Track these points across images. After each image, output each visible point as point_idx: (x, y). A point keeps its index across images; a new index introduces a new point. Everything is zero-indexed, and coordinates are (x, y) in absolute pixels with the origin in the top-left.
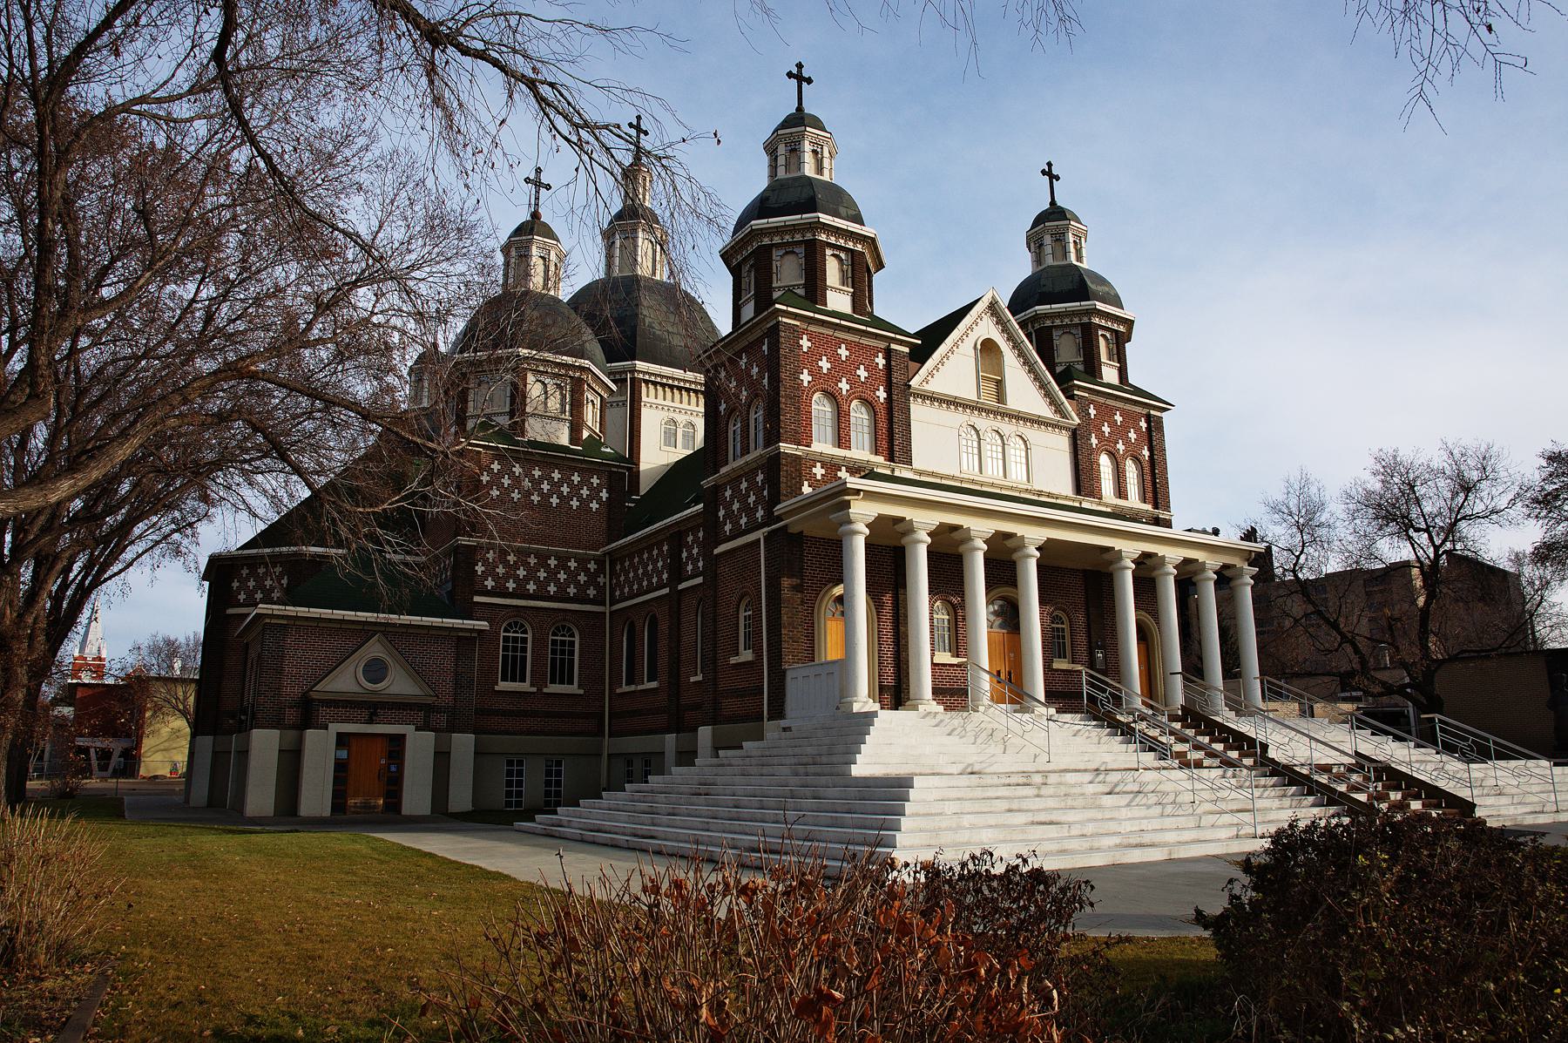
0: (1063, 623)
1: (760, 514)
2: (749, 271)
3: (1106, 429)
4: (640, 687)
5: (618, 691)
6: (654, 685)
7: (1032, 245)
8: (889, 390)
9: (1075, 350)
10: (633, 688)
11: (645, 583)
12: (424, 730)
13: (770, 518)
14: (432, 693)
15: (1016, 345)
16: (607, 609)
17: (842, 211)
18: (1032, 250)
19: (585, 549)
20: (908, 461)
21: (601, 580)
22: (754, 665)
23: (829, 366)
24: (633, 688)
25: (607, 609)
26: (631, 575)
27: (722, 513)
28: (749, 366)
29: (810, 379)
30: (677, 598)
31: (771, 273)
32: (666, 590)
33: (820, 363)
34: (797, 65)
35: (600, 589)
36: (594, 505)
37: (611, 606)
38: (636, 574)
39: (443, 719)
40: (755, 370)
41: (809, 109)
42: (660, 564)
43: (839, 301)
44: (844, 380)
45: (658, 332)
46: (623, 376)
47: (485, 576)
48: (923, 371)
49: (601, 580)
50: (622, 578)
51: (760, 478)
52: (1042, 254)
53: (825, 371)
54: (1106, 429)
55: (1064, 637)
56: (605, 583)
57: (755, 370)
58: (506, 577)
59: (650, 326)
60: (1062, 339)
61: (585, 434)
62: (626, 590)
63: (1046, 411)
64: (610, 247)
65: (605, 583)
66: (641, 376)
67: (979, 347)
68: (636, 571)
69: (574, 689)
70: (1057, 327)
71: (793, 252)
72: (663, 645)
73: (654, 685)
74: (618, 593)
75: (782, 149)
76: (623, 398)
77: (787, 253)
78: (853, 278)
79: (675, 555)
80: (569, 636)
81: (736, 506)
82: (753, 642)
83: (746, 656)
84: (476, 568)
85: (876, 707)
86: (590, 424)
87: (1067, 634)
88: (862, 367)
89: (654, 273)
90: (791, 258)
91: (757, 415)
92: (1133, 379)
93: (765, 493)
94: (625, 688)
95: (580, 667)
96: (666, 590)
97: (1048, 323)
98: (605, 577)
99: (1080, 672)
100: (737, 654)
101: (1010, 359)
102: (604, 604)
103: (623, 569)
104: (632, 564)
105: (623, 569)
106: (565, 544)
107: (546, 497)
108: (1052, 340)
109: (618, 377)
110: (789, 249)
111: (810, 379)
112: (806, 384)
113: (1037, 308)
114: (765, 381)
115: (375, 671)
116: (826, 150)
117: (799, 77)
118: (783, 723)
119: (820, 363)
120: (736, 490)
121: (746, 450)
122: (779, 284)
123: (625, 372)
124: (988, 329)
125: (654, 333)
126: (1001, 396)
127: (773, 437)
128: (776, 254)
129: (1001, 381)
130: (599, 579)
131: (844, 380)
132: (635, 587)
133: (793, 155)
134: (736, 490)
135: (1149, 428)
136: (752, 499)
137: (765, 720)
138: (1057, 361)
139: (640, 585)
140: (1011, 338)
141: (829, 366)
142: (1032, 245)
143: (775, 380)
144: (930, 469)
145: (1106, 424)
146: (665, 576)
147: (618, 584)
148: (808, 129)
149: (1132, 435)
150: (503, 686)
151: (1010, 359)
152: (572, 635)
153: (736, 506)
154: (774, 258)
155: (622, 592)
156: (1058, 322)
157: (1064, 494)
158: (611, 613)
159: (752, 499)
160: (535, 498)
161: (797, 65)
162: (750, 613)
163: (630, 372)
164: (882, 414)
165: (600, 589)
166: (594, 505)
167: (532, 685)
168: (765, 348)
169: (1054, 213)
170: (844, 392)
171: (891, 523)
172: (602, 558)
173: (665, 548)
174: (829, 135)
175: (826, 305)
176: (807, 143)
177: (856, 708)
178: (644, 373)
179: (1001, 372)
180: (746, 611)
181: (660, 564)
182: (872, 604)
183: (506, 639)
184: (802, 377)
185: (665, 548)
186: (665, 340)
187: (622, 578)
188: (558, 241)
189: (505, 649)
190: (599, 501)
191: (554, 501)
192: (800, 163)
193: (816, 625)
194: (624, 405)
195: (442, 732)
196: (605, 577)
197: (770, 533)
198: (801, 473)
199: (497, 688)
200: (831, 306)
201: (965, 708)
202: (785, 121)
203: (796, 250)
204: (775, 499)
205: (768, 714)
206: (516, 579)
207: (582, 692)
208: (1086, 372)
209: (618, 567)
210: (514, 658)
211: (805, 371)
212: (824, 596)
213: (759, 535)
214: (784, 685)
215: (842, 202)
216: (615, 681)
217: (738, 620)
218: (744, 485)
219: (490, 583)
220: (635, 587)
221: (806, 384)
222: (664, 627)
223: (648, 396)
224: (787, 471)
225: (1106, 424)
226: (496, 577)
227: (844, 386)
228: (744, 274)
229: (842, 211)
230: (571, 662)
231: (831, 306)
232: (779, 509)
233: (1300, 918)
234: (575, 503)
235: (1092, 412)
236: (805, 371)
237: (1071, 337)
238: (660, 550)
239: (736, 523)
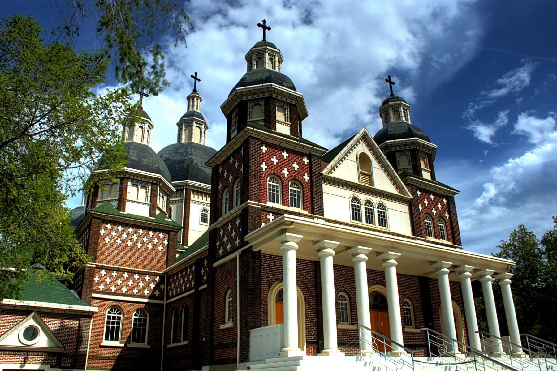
0: (409, 306)
1: (238, 241)
2: (235, 116)
3: (426, 202)
4: (179, 344)
5: (169, 346)
6: (186, 343)
7: (383, 114)
8: (311, 176)
9: (407, 163)
10: (175, 345)
11: (183, 288)
12: (56, 367)
13: (243, 243)
14: (62, 346)
15: (378, 157)
16: (164, 302)
17: (284, 84)
18: (383, 116)
19: (154, 270)
20: (321, 212)
21: (162, 287)
22: (232, 330)
23: (277, 161)
24: (175, 345)
25: (164, 302)
26: (177, 283)
27: (218, 244)
28: (234, 163)
29: (266, 167)
30: (198, 294)
31: (247, 114)
32: (193, 291)
33: (272, 160)
34: (263, 21)
35: (161, 292)
36: (160, 248)
37: (167, 300)
38: (179, 282)
39: (69, 361)
40: (237, 164)
41: (268, 40)
42: (191, 277)
43: (283, 129)
44: (285, 169)
45: (200, 167)
46: (182, 188)
47: (99, 283)
48: (329, 166)
49: (162, 287)
50: (173, 286)
51: (238, 222)
52: (388, 118)
53: (275, 164)
54: (426, 202)
55: (410, 314)
56: (164, 288)
57: (237, 164)
58: (111, 284)
59: (196, 164)
60: (400, 157)
61: (158, 212)
62: (174, 292)
63: (393, 190)
64: (180, 130)
65: (164, 288)
66: (190, 188)
67: (358, 157)
68: (179, 282)
69: (145, 345)
70: (398, 151)
71: (258, 104)
72: (190, 320)
73: (186, 343)
74: (170, 294)
75: (254, 57)
76: (182, 198)
77: (255, 105)
78: (290, 117)
79: (198, 271)
80: (144, 316)
81: (225, 239)
82: (233, 318)
83: (229, 325)
84: (95, 279)
85: (303, 353)
86: (161, 206)
87: (412, 312)
88: (295, 163)
89: (200, 142)
90: (258, 107)
91: (237, 188)
92: (438, 179)
93: (240, 230)
94: (172, 345)
95: (149, 333)
96: (193, 291)
97: (393, 149)
98: (164, 285)
99: (426, 330)
100: (224, 323)
101: (375, 164)
102: (163, 300)
103: (173, 281)
104: (177, 278)
105: (173, 281)
106: (143, 266)
107: (135, 242)
108: (396, 158)
109: (179, 188)
110: (256, 102)
111: (266, 167)
112: (264, 170)
113: (387, 141)
114: (242, 170)
115: (31, 333)
116: (277, 58)
117: (264, 26)
118: (247, 364)
119: (272, 160)
120: (225, 229)
121: (231, 207)
122: (251, 120)
123: (183, 186)
124: (362, 148)
125: (198, 167)
126: (371, 182)
127: (245, 196)
128: (249, 105)
129: (371, 175)
130: (161, 286)
131: (285, 169)
132: (179, 290)
133: (260, 60)
134: (225, 229)
135: (448, 203)
136: (234, 234)
137: (238, 362)
138: (398, 168)
139: (181, 289)
140: (375, 153)
141: (277, 161)
142: (383, 114)
143: (247, 167)
144: (334, 219)
145: (426, 199)
146: (193, 283)
147: (171, 289)
148: (268, 47)
149: (440, 206)
150: (105, 343)
151: (375, 164)
152: (146, 316)
153: (225, 239)
154: (248, 107)
155: (172, 293)
156: (398, 149)
157: (407, 235)
158: (166, 304)
159: (234, 234)
160: (129, 243)
161: (263, 21)
162: (231, 299)
163: (185, 185)
164: (307, 188)
165: (161, 292)
166: (160, 248)
167: (121, 343)
168: (242, 152)
169: (393, 98)
170: (286, 176)
171: (312, 244)
172: (163, 275)
173: (194, 268)
174: (278, 51)
175: (276, 130)
176: (267, 54)
177: (291, 355)
178: (192, 186)
179: (370, 170)
180: (229, 298)
181: (191, 277)
182: (300, 290)
183: (109, 317)
184: (262, 166)
185: (194, 268)
186: (203, 171)
187: (173, 286)
188: (150, 119)
189: (108, 322)
190: (163, 245)
191: (139, 245)
192: (263, 63)
193: (268, 305)
194: (182, 202)
195: (68, 368)
196: (164, 285)
197: (242, 251)
198: (260, 218)
199: (102, 344)
200: (278, 130)
201: (356, 354)
202: (256, 44)
203: (260, 103)
204: (246, 231)
205: (240, 358)
206: (116, 285)
207: (149, 347)
208: (414, 173)
209: (171, 280)
210: (113, 328)
211: (264, 163)
212: (273, 288)
213: (237, 254)
214: (249, 341)
215: (285, 80)
216: (167, 341)
217: (225, 303)
218: (230, 227)
219: (102, 287)
220: (179, 290)
221: (264, 170)
222: (191, 311)
223: (194, 197)
224: (252, 216)
225: (426, 199)
226: (105, 284)
227: (285, 172)
228: (233, 117)
229: (284, 84)
230: (144, 330)
231: (278, 130)
232: (247, 238)
233: (61, 223)
234: (150, 246)
235: (419, 193)
236: (264, 163)
237: (405, 156)
238: (191, 269)
239: (225, 249)
